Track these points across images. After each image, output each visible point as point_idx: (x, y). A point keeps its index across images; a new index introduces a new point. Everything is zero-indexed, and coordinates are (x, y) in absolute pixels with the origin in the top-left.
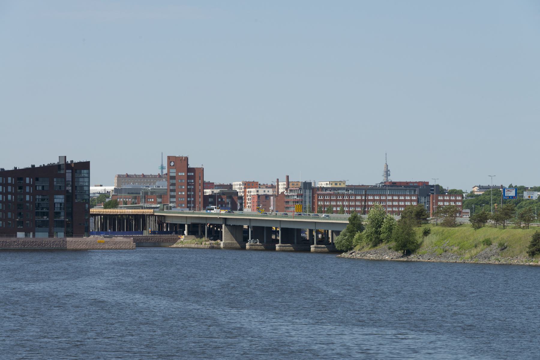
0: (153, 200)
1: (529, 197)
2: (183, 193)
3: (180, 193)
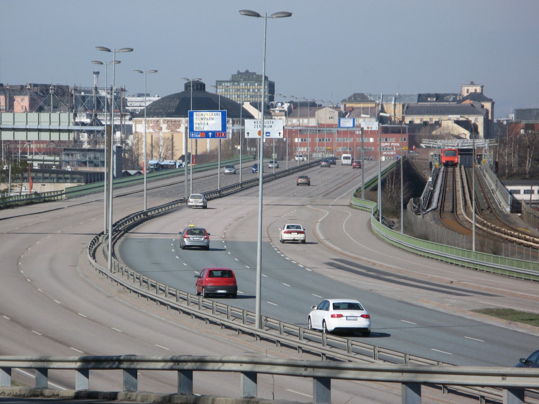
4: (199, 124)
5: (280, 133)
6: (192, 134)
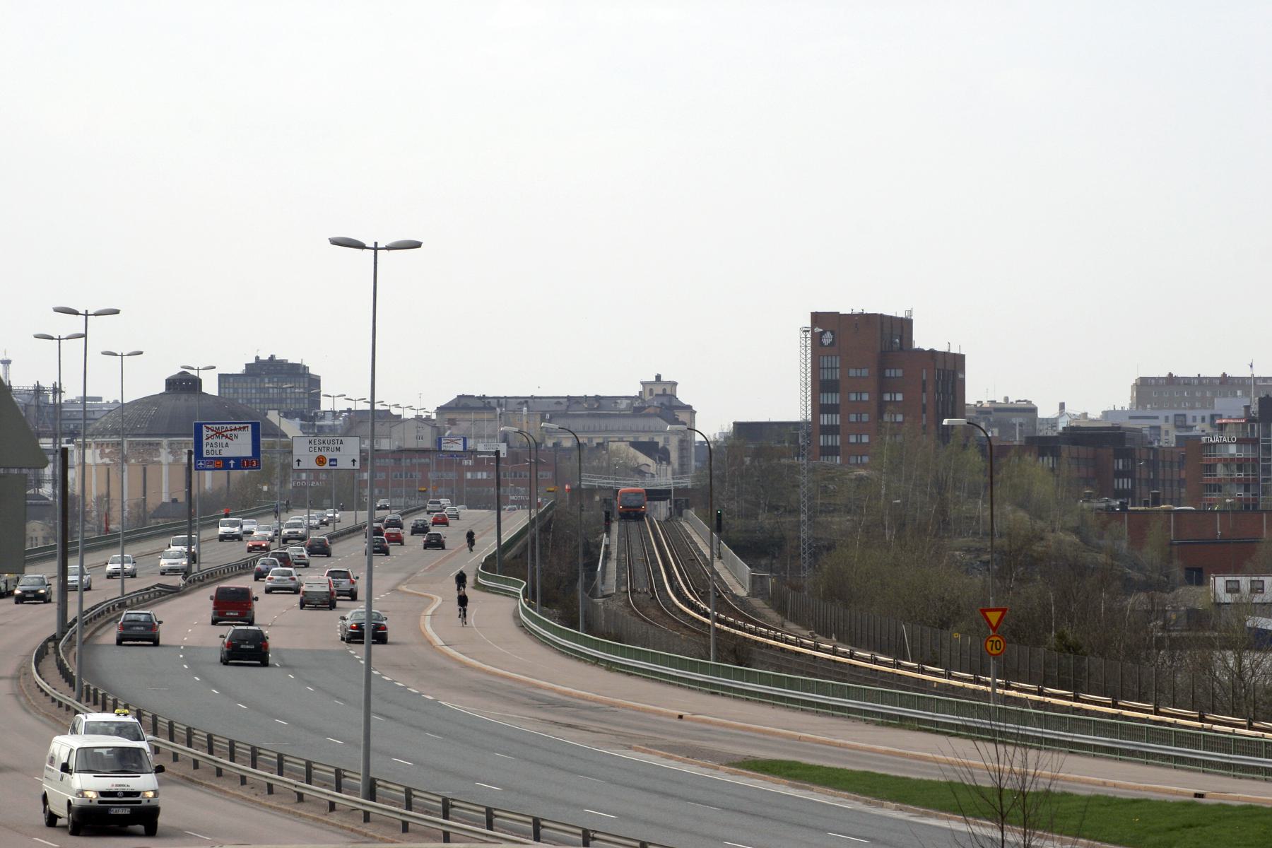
0: (899, 397)
1: (320, 460)
2: (865, 397)
3: (853, 397)
4: (212, 446)
5: (354, 461)
6: (199, 462)
